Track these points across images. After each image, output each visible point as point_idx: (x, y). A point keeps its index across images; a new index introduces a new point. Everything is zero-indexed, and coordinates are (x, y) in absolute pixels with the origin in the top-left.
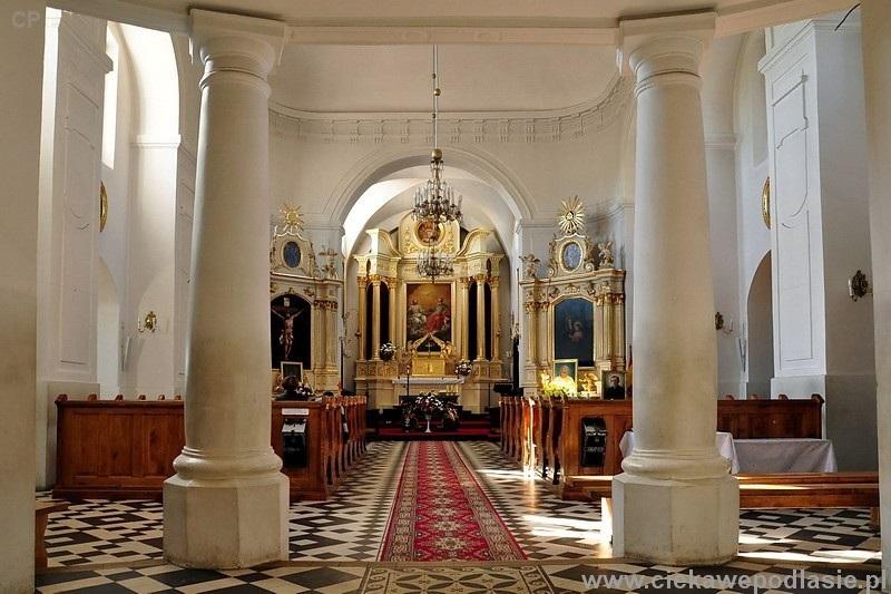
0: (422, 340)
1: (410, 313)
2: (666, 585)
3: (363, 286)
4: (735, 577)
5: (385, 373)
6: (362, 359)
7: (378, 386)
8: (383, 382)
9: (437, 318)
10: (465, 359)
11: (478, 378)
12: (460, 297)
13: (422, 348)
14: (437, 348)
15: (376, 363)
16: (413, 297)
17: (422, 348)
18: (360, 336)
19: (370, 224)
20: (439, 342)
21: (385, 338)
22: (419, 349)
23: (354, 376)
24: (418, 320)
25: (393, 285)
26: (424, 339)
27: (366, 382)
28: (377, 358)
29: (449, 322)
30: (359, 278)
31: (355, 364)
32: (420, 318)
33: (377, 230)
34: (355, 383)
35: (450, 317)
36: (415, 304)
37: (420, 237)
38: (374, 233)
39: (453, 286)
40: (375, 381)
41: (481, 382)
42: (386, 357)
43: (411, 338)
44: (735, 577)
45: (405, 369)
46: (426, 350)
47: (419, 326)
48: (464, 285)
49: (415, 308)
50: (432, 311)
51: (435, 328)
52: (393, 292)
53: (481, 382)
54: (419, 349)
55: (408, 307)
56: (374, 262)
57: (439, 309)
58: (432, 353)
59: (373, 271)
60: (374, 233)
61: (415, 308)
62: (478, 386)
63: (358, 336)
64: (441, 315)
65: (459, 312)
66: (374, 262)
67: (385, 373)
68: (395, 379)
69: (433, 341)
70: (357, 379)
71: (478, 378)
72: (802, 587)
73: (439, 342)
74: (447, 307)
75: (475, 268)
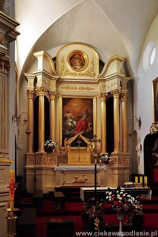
0: (74, 138)
1: (65, 119)
2: (98, 235)
3: (31, 97)
4: (116, 232)
5: (49, 163)
6: (31, 152)
7: (44, 172)
8: (47, 169)
9: (84, 123)
10: (104, 152)
11: (116, 166)
12: (99, 109)
13: (74, 144)
14: (84, 144)
15: (42, 154)
16: (67, 108)
17: (74, 144)
18: (30, 133)
19: (36, 48)
20: (86, 140)
21: (48, 136)
22: (73, 145)
23: (25, 165)
24: (70, 124)
25: (53, 97)
26: (76, 137)
27: (34, 170)
28: (42, 151)
29: (92, 126)
30: (28, 91)
31: (26, 156)
32: (72, 122)
33: (42, 52)
34: (25, 170)
35: (92, 122)
36: (68, 112)
37: (72, 65)
38: (39, 55)
39: (94, 100)
40: (41, 169)
41: (119, 169)
42: (48, 150)
43: (66, 136)
44: (116, 232)
45: (64, 159)
46: (76, 145)
47: (72, 128)
48: (103, 99)
49: (69, 115)
50: (80, 118)
51: (82, 129)
52: (53, 102)
53: (119, 169)
54: (73, 145)
55: (63, 115)
56: (40, 78)
57: (84, 117)
58: (81, 148)
59: (39, 84)
60: (39, 55)
61: (69, 115)
62: (116, 172)
63: (28, 133)
64: (86, 121)
65: (99, 120)
66: (40, 78)
67: (49, 163)
68: (56, 167)
69: (81, 139)
70: (27, 166)
71: (116, 166)
72: (134, 235)
73: (86, 140)
74: (90, 116)
75: (112, 86)
